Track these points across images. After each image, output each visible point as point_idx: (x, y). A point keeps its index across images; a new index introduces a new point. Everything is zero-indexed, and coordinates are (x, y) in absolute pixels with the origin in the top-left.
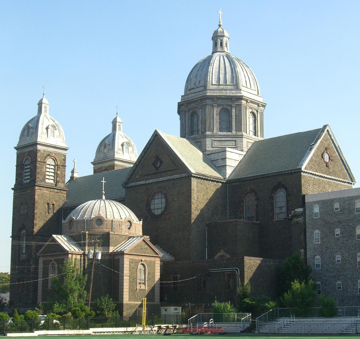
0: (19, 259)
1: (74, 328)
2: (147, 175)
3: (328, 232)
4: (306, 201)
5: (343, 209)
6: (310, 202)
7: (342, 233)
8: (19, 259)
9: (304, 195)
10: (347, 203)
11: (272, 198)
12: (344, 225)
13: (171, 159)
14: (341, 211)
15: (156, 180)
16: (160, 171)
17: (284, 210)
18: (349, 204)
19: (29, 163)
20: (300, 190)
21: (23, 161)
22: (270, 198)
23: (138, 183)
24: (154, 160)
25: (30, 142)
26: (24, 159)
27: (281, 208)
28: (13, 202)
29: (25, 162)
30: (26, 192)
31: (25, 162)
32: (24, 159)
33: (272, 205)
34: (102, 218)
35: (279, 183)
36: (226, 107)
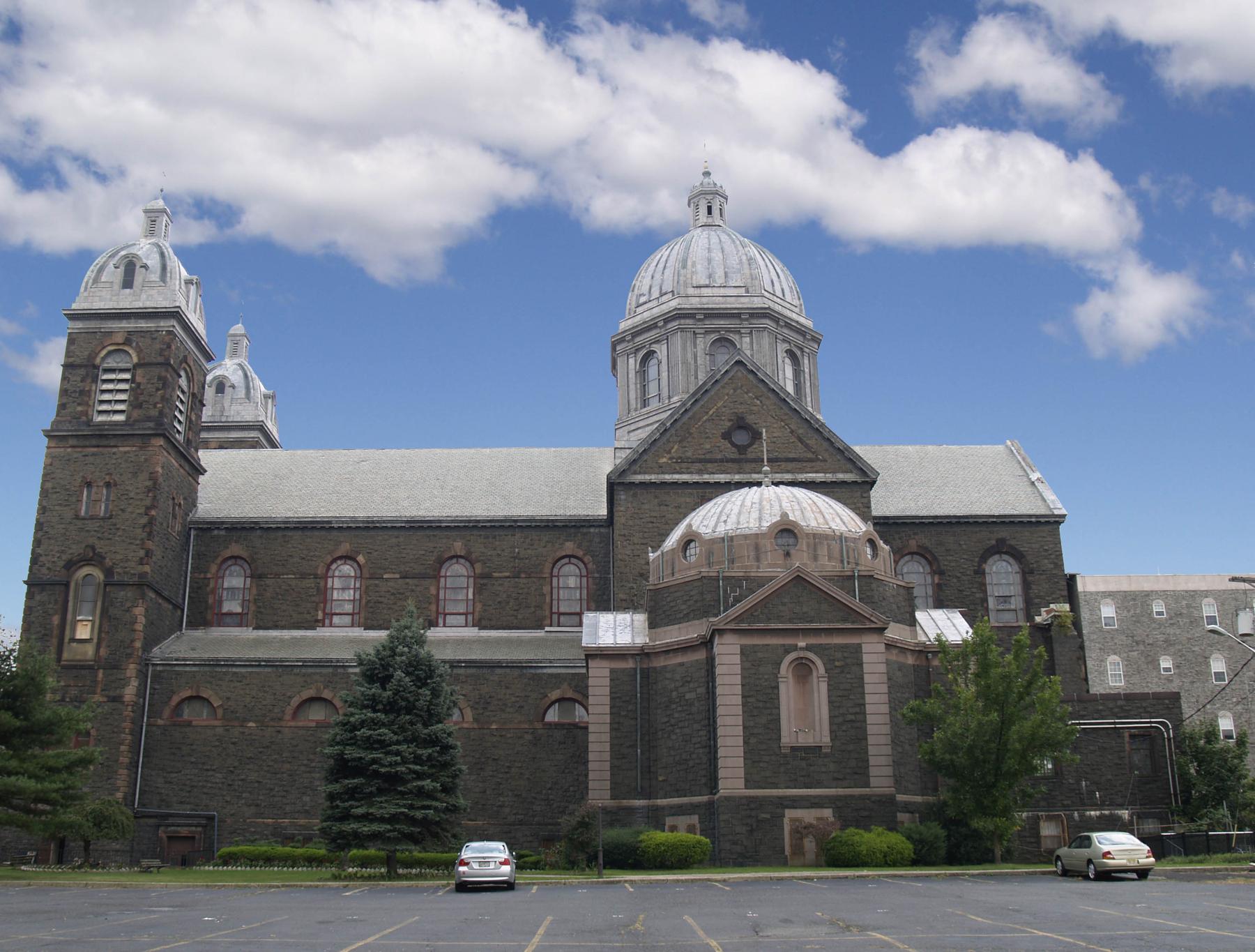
0: (59, 659)
1: (765, 798)
2: (700, 461)
3: (904, 715)
4: (1080, 588)
5: (1175, 615)
6: (1091, 593)
7: (1177, 666)
8: (59, 659)
9: (1072, 578)
10: (1184, 603)
11: (981, 573)
12: (1180, 650)
13: (792, 432)
14: (1171, 618)
15: (696, 478)
16: (750, 456)
17: (1017, 603)
18: (1188, 606)
19: (129, 365)
20: (1058, 563)
21: (97, 354)
22: (976, 572)
23: (668, 477)
24: (729, 424)
25: (148, 304)
26: (104, 352)
27: (1006, 599)
28: (42, 472)
29: (103, 359)
30: (115, 450)
31: (103, 359)
32: (104, 352)
33: (983, 587)
34: (795, 524)
35: (1001, 542)
36: (795, 349)
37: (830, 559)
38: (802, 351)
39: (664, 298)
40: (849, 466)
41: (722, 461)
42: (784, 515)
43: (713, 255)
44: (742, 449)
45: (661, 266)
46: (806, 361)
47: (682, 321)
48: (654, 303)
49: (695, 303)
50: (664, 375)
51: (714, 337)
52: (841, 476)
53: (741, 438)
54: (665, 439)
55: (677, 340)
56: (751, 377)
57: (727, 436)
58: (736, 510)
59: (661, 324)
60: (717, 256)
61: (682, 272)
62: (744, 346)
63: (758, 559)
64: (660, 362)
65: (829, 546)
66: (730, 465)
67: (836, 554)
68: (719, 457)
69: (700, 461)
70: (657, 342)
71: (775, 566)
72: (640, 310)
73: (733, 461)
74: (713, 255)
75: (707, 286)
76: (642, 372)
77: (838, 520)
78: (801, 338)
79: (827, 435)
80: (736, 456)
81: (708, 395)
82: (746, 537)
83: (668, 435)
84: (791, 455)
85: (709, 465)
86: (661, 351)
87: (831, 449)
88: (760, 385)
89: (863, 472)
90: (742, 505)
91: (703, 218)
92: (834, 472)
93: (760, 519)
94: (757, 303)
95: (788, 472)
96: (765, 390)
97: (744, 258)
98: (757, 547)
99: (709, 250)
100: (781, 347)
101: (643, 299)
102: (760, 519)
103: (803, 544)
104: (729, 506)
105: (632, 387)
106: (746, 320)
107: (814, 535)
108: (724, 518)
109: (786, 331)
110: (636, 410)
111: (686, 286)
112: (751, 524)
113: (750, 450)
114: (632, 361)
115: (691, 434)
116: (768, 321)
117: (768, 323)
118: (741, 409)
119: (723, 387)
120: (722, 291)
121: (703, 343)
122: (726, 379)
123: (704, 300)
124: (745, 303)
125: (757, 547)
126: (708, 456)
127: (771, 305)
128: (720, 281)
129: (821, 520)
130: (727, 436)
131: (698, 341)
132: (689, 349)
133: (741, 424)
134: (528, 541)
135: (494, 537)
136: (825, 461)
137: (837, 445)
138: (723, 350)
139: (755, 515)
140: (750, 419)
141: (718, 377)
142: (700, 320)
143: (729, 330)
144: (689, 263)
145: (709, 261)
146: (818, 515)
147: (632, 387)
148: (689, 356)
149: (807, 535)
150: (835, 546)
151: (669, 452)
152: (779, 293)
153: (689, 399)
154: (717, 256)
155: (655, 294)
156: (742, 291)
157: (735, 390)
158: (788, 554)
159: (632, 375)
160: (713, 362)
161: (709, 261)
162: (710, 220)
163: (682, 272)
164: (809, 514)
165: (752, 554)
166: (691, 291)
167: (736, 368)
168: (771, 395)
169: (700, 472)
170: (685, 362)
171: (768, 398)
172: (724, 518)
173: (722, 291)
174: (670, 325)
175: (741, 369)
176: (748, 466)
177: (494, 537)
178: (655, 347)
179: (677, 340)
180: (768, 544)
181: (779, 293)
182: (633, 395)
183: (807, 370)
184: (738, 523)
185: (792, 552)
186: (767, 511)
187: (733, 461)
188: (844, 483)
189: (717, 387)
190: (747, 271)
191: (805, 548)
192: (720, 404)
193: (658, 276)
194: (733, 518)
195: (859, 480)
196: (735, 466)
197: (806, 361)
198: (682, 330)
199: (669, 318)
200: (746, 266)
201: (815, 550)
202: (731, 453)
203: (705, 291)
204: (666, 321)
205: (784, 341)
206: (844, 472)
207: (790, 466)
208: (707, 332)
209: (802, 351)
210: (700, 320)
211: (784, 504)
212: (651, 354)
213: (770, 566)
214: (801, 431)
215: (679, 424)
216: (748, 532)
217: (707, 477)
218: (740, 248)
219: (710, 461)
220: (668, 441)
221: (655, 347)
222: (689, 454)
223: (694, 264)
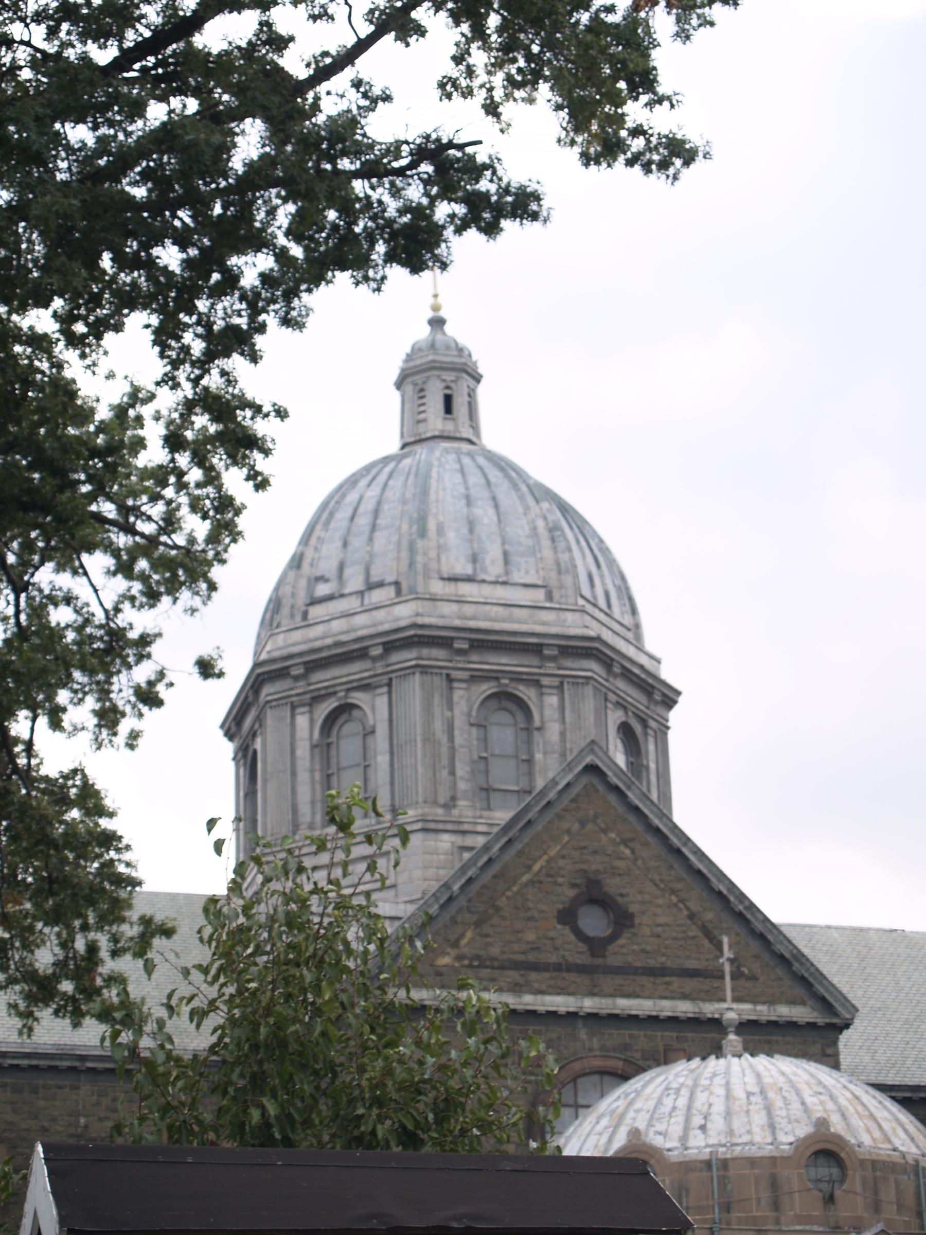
2: (517, 966)
13: (692, 916)
24: (572, 893)
37: (901, 1207)
38: (645, 725)
39: (377, 596)
40: (799, 991)
41: (558, 968)
42: (822, 1123)
43: (477, 511)
44: (597, 946)
45: (363, 521)
46: (651, 747)
47: (425, 652)
48: (351, 604)
49: (446, 615)
50: (382, 760)
51: (487, 688)
52: (784, 1012)
53: (594, 922)
54: (447, 916)
55: (413, 690)
56: (613, 799)
57: (567, 916)
58: (719, 1107)
59: (376, 652)
60: (485, 514)
61: (420, 544)
62: (548, 712)
63: (776, 1205)
64: (370, 732)
65: (898, 1184)
66: (573, 977)
67: (910, 1200)
68: (553, 959)
69: (517, 966)
70: (365, 687)
71: (809, 1220)
72: (316, 612)
73: (581, 969)
74: (477, 511)
75: (470, 579)
76: (324, 747)
77: (902, 1135)
78: (643, 699)
79: (759, 927)
80: (583, 959)
81: (531, 833)
82: (752, 1162)
83: (453, 908)
84: (692, 964)
85: (533, 976)
86: (375, 708)
87: (766, 956)
88: (632, 818)
89: (825, 1005)
90: (729, 1096)
91: (436, 422)
92: (754, 1002)
93: (772, 1127)
94: (574, 625)
95: (685, 997)
96: (640, 828)
97: (540, 524)
98: (774, 1184)
99: (469, 501)
100: (615, 717)
101: (322, 590)
102: (772, 1127)
103: (855, 1181)
104: (701, 1098)
105: (303, 776)
106: (553, 659)
107: (874, 1163)
108: (697, 1120)
109: (621, 684)
110: (311, 827)
111: (427, 576)
112: (754, 1136)
113: (612, 948)
114: (302, 721)
115: (498, 909)
116: (594, 665)
117: (594, 668)
118: (595, 864)
119: (560, 817)
120: (501, 593)
121: (467, 699)
122: (565, 802)
123: (468, 610)
124: (548, 623)
125: (774, 1184)
126: (531, 957)
127: (607, 636)
128: (494, 570)
129: (877, 1134)
130: (567, 916)
131: (458, 695)
132: (437, 711)
133: (594, 894)
134: (106, 1101)
135: (35, 1091)
136: (753, 978)
137: (780, 948)
138: (504, 717)
139: (759, 1118)
140: (613, 885)
141: (552, 795)
142: (461, 652)
143: (517, 678)
144: (432, 526)
145: (471, 525)
146: (870, 1123)
147: (303, 776)
148: (438, 726)
149: (863, 1162)
150: (907, 1181)
151: (456, 944)
152: (602, 603)
153: (498, 837)
154: (485, 514)
155: (355, 582)
156: (539, 596)
157: (583, 823)
158: (830, 1199)
159: (303, 751)
160: (485, 741)
161: (471, 525)
162: (449, 427)
163: (420, 544)
164: (856, 1121)
165: (766, 1195)
166: (437, 587)
167: (585, 780)
168: (650, 838)
169: (517, 989)
170: (430, 739)
171: (646, 844)
172: (697, 1120)
173: (501, 593)
174: (395, 657)
175: (596, 781)
176: (608, 982)
177: (35, 1091)
178: (358, 698)
179: (413, 690)
180: (793, 1178)
181: (602, 603)
182: (304, 794)
183: (652, 766)
184: (731, 1132)
185: (838, 1193)
186: (780, 1113)
187: (581, 969)
188: (792, 1025)
189: (550, 815)
190: (548, 553)
191: (858, 1188)
192: (553, 852)
193: (358, 542)
194: (717, 1124)
195: (820, 1021)
196: (583, 980)
197: (651, 747)
198: (424, 670)
199: (396, 641)
200: (546, 543)
201: (876, 1192)
202: (577, 953)
203: (466, 589)
204: (390, 647)
205: (618, 705)
206: (792, 1002)
207: (690, 984)
208: (476, 678)
209: (645, 725)
210: (461, 652)
211: (809, 1100)
212: (346, 709)
213: (800, 1219)
214: (709, 916)
215: (475, 887)
216: (754, 1152)
217: (529, 1001)
218: (531, 502)
219: (536, 967)
220: (454, 921)
221: (358, 698)
222: (495, 951)
223: (440, 531)
